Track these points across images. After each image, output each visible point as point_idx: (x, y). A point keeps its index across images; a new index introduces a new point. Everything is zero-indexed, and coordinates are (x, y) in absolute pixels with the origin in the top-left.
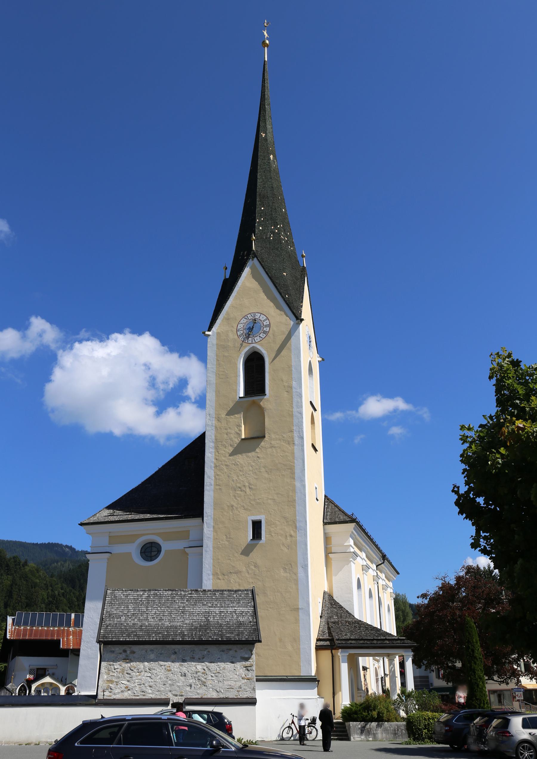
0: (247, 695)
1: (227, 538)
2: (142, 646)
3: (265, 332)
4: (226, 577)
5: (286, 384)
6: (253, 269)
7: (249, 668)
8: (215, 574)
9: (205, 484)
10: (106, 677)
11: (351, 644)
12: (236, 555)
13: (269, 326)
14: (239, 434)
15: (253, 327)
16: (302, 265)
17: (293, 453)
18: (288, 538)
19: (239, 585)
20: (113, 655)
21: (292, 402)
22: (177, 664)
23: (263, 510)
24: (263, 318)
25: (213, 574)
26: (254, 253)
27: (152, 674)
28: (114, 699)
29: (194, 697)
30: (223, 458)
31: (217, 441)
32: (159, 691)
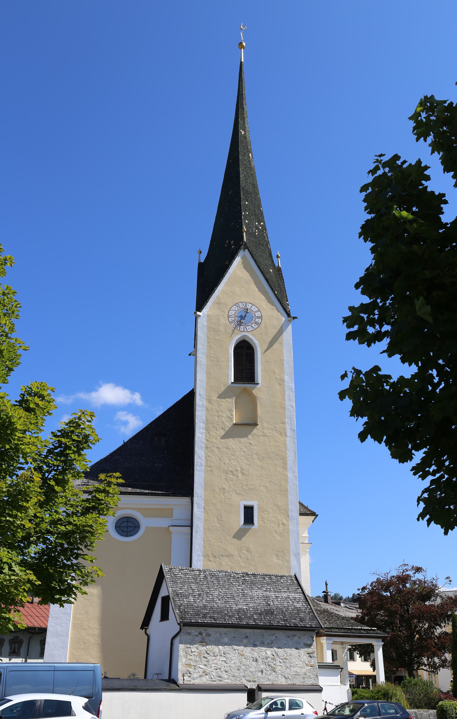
0: (311, 682)
1: (218, 520)
2: (216, 629)
3: (256, 323)
4: (217, 559)
5: (278, 377)
6: (243, 258)
7: (312, 655)
8: (206, 556)
9: (195, 464)
10: (184, 660)
11: (336, 632)
12: (228, 538)
13: (261, 317)
14: (231, 419)
15: (245, 316)
16: (277, 265)
17: (285, 444)
18: (281, 526)
19: (231, 568)
20: (189, 637)
21: (284, 394)
22: (249, 649)
23: (255, 496)
24: (254, 309)
25: (204, 556)
26: (245, 244)
27: (227, 658)
28: (193, 684)
29: (266, 683)
30: (215, 441)
31: (207, 422)
32: (234, 676)
